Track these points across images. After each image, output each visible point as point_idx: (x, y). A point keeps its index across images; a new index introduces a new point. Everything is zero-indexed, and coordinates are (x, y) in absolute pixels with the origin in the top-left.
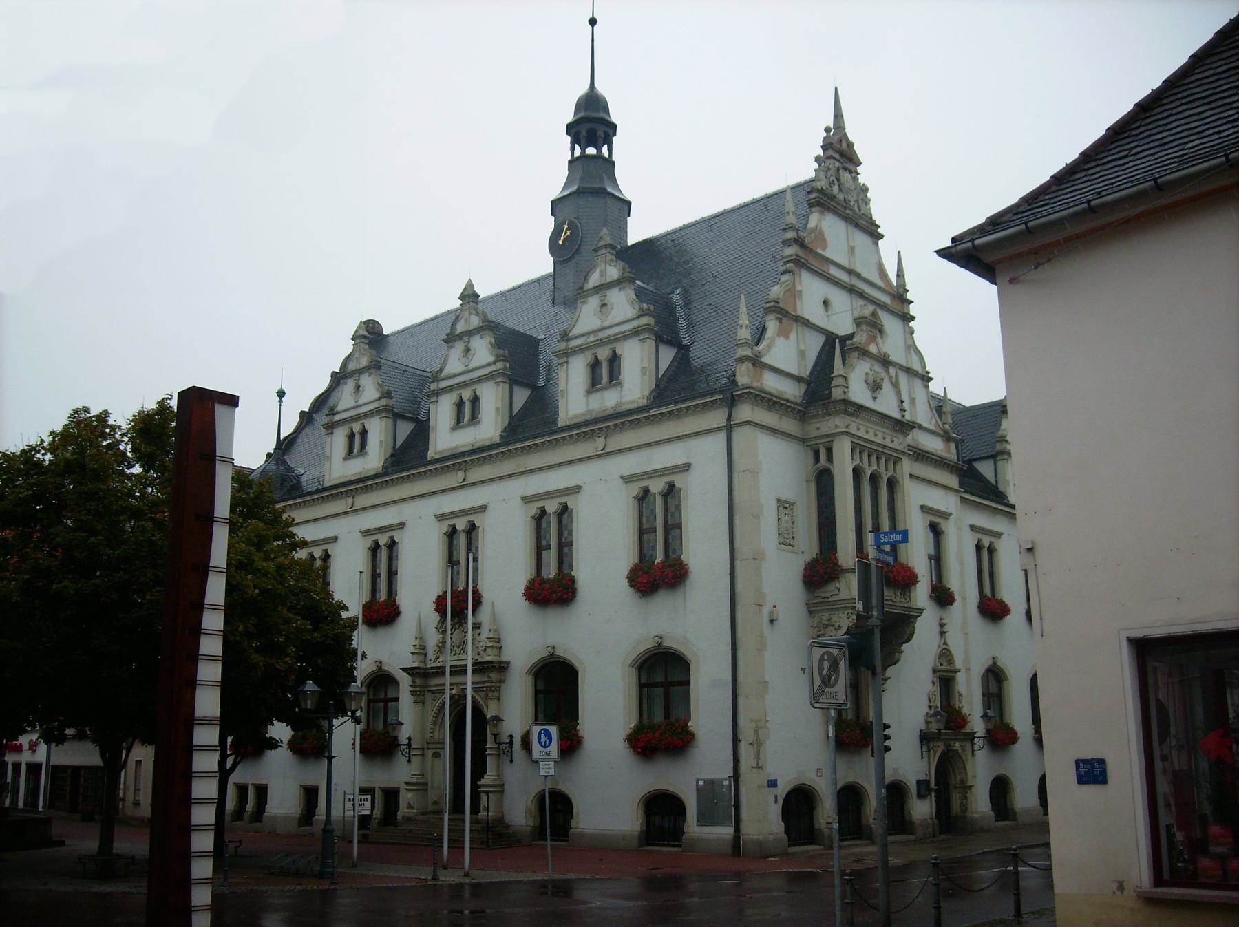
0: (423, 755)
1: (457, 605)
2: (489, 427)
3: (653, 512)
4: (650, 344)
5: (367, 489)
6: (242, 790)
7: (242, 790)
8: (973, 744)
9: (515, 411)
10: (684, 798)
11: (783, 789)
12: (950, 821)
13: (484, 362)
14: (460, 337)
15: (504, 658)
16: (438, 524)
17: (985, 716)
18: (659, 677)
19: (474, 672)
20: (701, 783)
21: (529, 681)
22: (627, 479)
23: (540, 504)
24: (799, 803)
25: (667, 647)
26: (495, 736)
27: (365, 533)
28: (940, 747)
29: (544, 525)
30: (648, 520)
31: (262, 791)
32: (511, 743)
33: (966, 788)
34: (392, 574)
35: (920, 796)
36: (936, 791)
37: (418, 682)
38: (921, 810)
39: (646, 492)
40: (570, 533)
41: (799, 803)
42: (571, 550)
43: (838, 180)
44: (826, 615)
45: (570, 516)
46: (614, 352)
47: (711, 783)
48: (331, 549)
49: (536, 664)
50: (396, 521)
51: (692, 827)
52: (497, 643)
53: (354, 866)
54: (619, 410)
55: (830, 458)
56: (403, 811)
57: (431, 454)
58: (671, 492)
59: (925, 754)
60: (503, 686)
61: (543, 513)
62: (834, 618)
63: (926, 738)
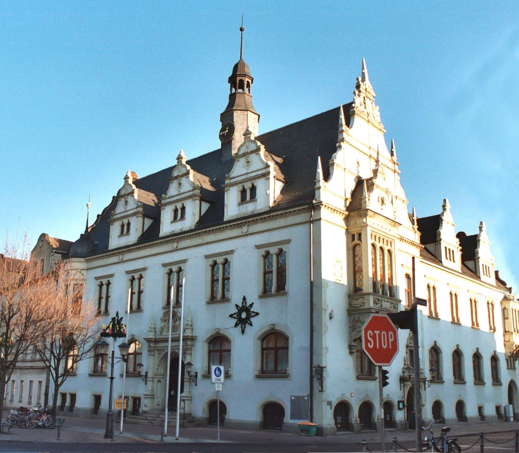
0: (153, 381)
1: (172, 308)
2: (190, 221)
3: (271, 264)
4: (140, 219)
5: (129, 251)
6: (64, 395)
7: (64, 395)
8: (425, 384)
9: (202, 214)
10: (284, 406)
11: (334, 404)
12: (413, 422)
13: (132, 208)
14: (123, 196)
15: (195, 334)
16: (95, 280)
17: (431, 370)
18: (217, 348)
19: (172, 341)
20: (293, 398)
21: (206, 346)
22: (258, 247)
23: (170, 267)
24: (342, 409)
25: (278, 330)
26: (189, 372)
27: (128, 272)
28: (409, 384)
29: (216, 269)
30: (268, 267)
31: (73, 397)
32: (196, 376)
33: (421, 406)
34: (226, 279)
35: (399, 409)
36: (407, 407)
37: (152, 345)
38: (400, 416)
39: (268, 253)
40: (229, 273)
41: (342, 409)
42: (228, 282)
43: (365, 103)
44: (357, 316)
45: (229, 265)
46: (253, 185)
47: (298, 398)
48: (111, 280)
49: (209, 338)
50: (143, 267)
51: (288, 419)
52: (190, 326)
53: (120, 433)
54: (255, 213)
55: (360, 239)
56: (143, 408)
57: (226, 219)
58: (281, 253)
59: (402, 388)
60: (193, 348)
61: (215, 263)
62: (361, 318)
63: (402, 380)
